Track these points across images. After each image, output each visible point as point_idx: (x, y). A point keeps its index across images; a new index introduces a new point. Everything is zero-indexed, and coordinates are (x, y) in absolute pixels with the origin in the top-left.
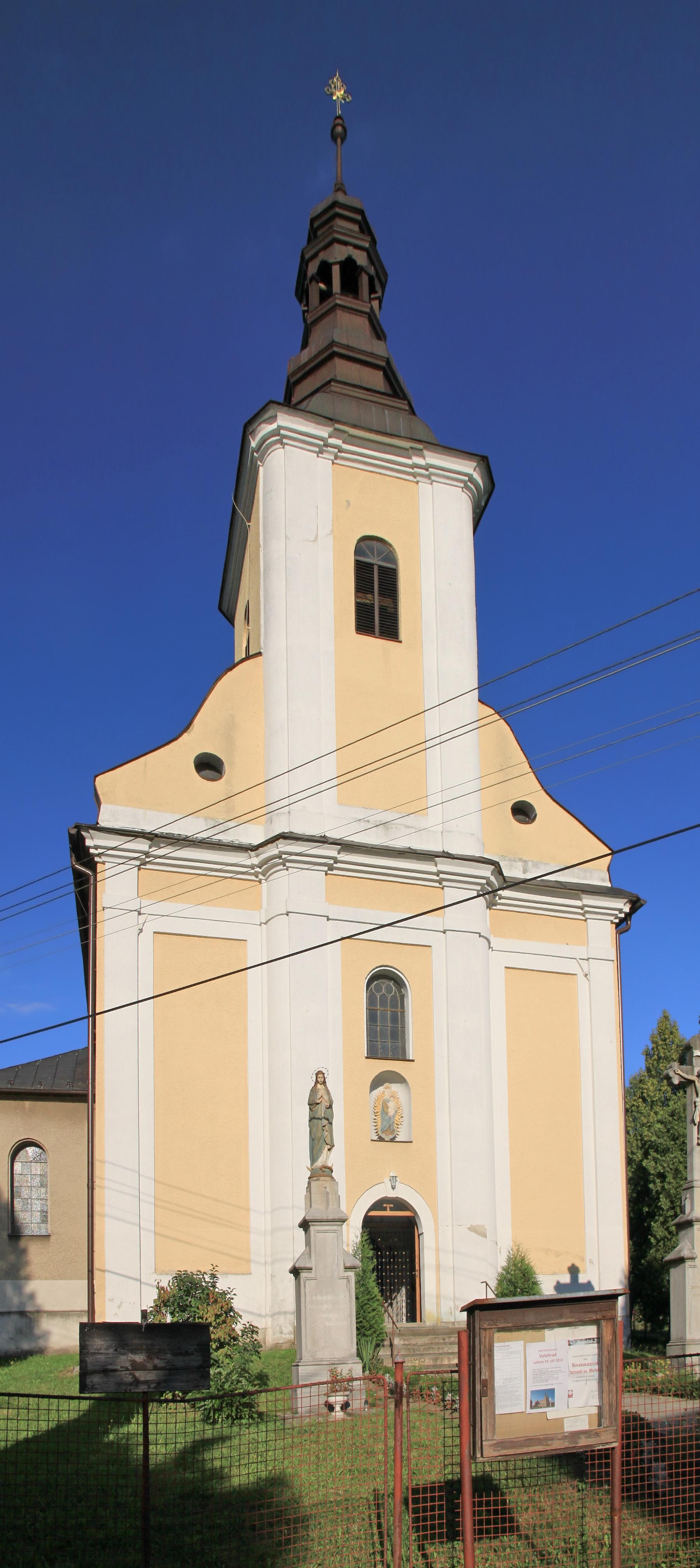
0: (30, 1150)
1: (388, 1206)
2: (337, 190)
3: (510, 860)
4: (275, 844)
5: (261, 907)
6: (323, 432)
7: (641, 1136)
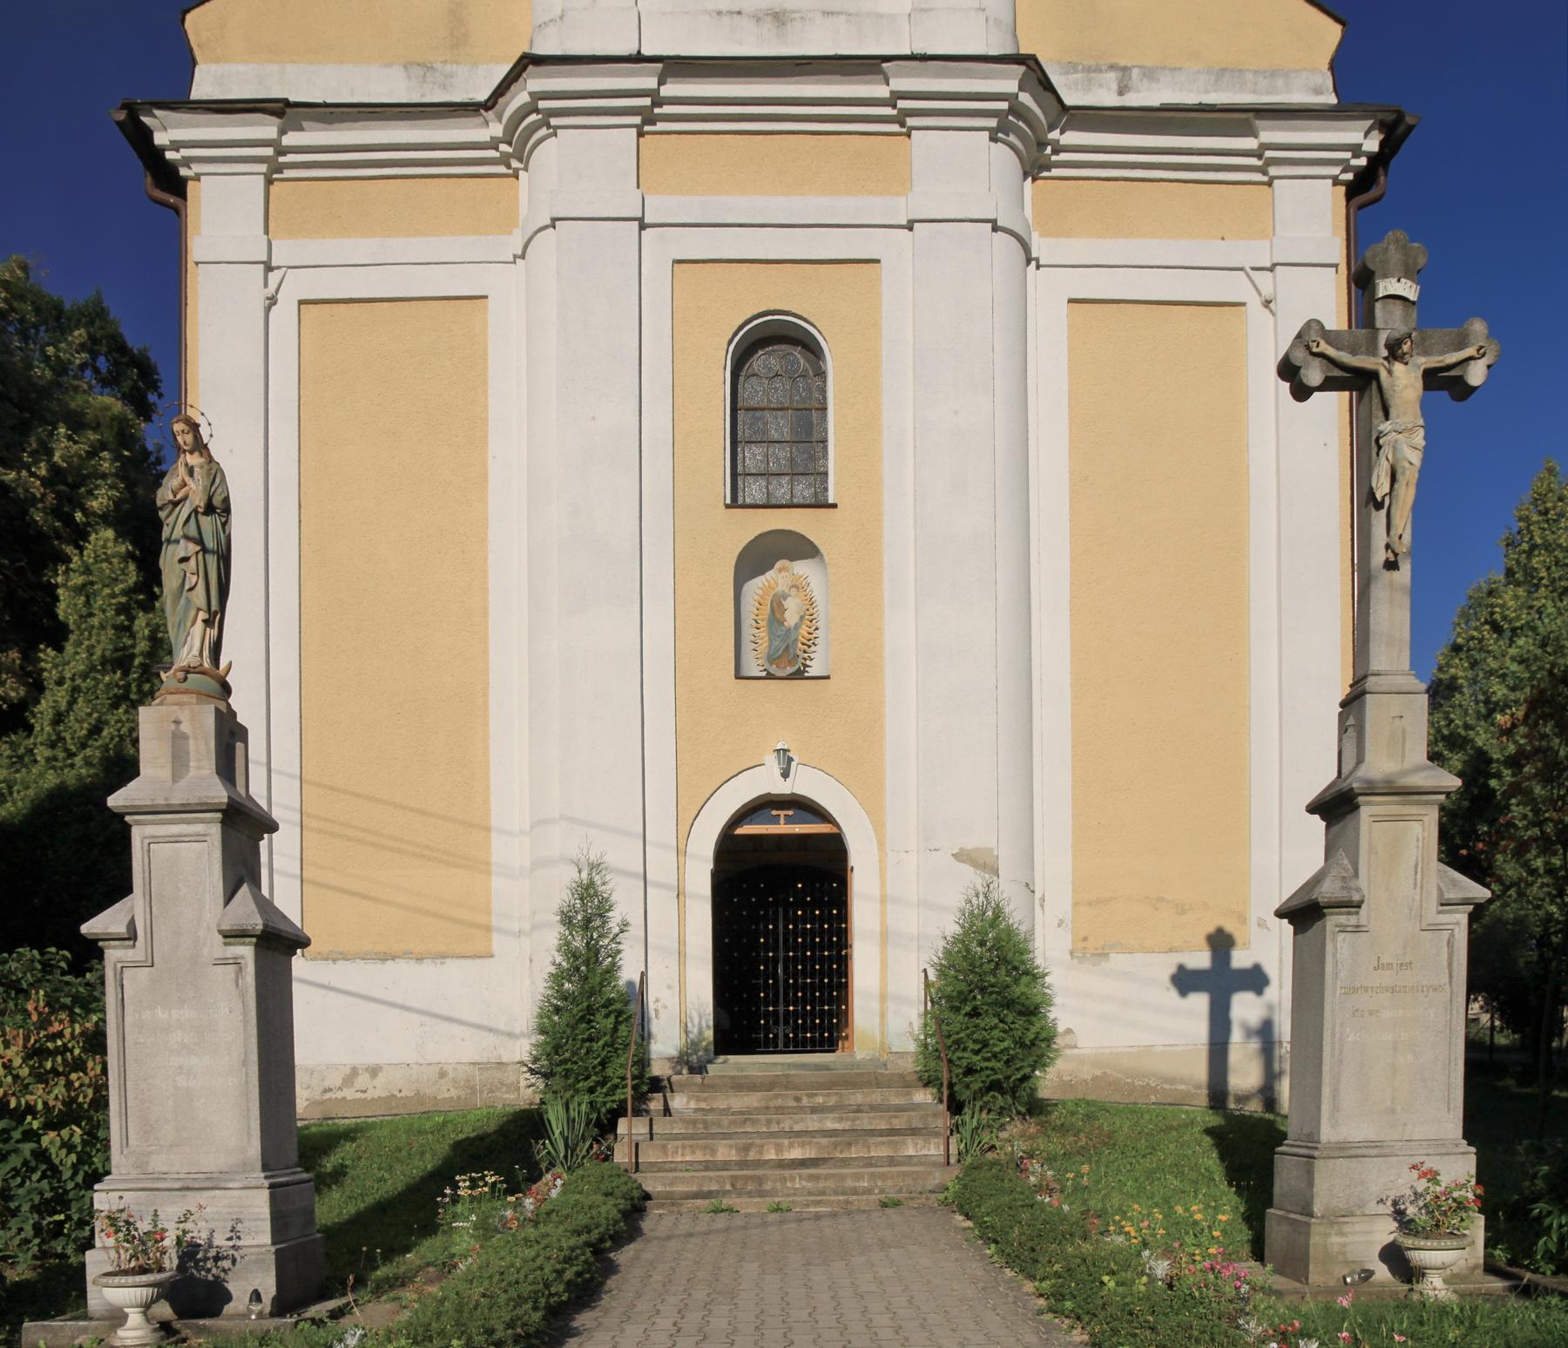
1: (783, 813)
3: (1088, 70)
7: (1485, 693)
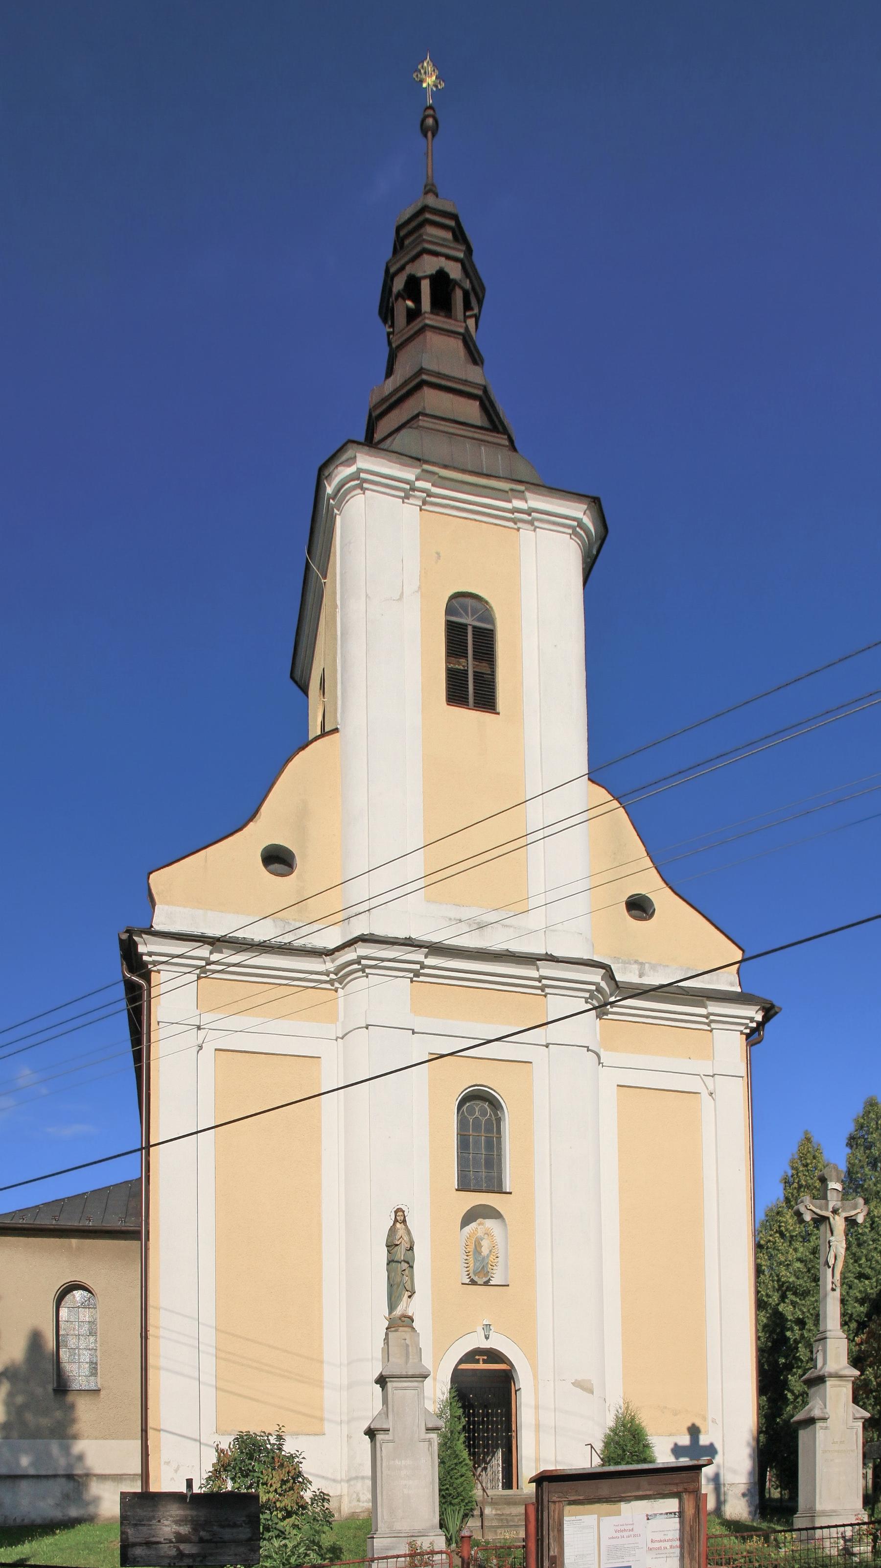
0: (78, 1294)
1: (481, 1358)
2: (426, 193)
3: (624, 962)
4: (353, 947)
5: (337, 1020)
6: (409, 474)
7: (778, 1276)
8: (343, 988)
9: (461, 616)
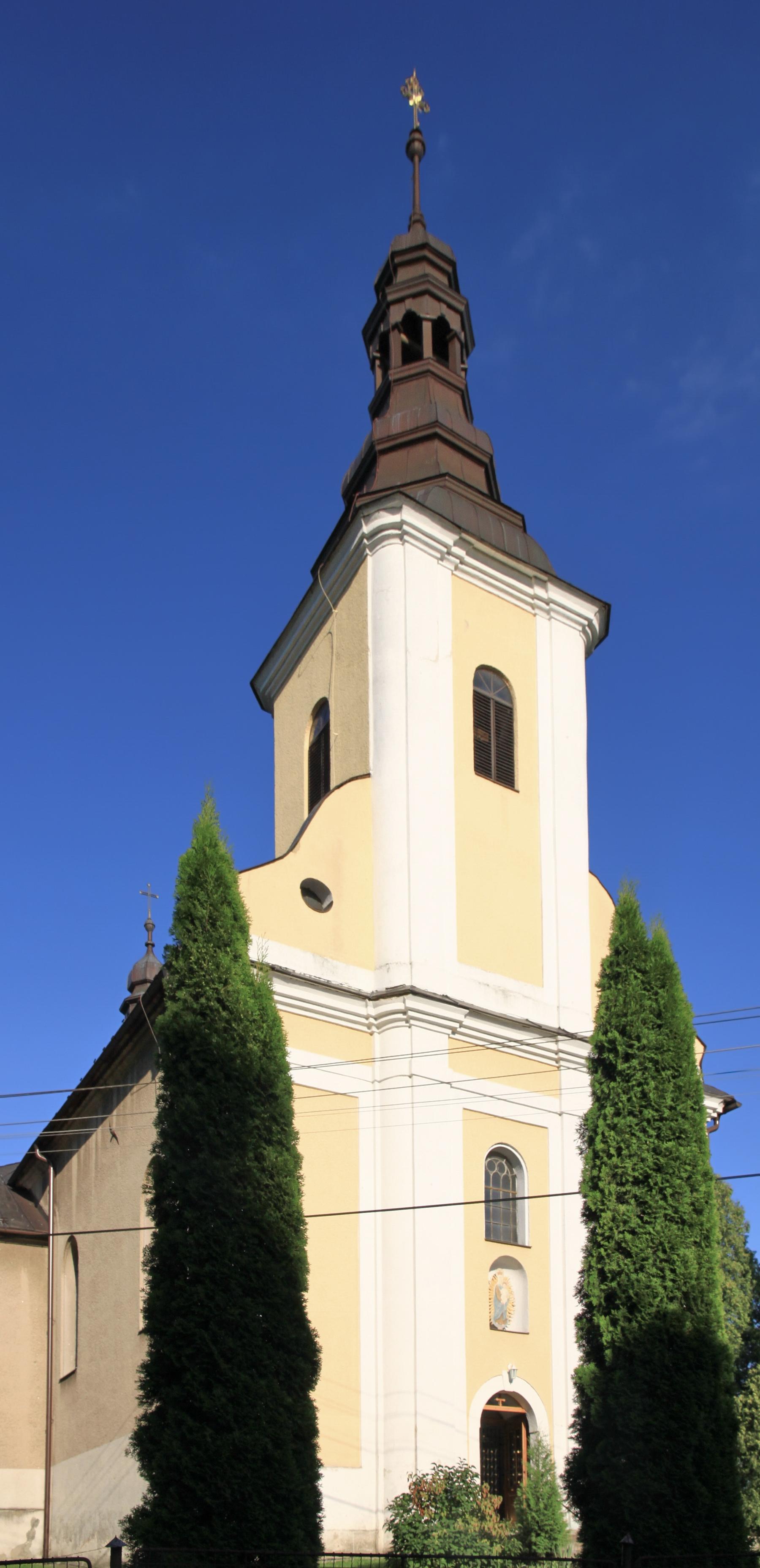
4: (401, 998)
6: (449, 538)
8: (379, 1033)
9: (485, 689)
